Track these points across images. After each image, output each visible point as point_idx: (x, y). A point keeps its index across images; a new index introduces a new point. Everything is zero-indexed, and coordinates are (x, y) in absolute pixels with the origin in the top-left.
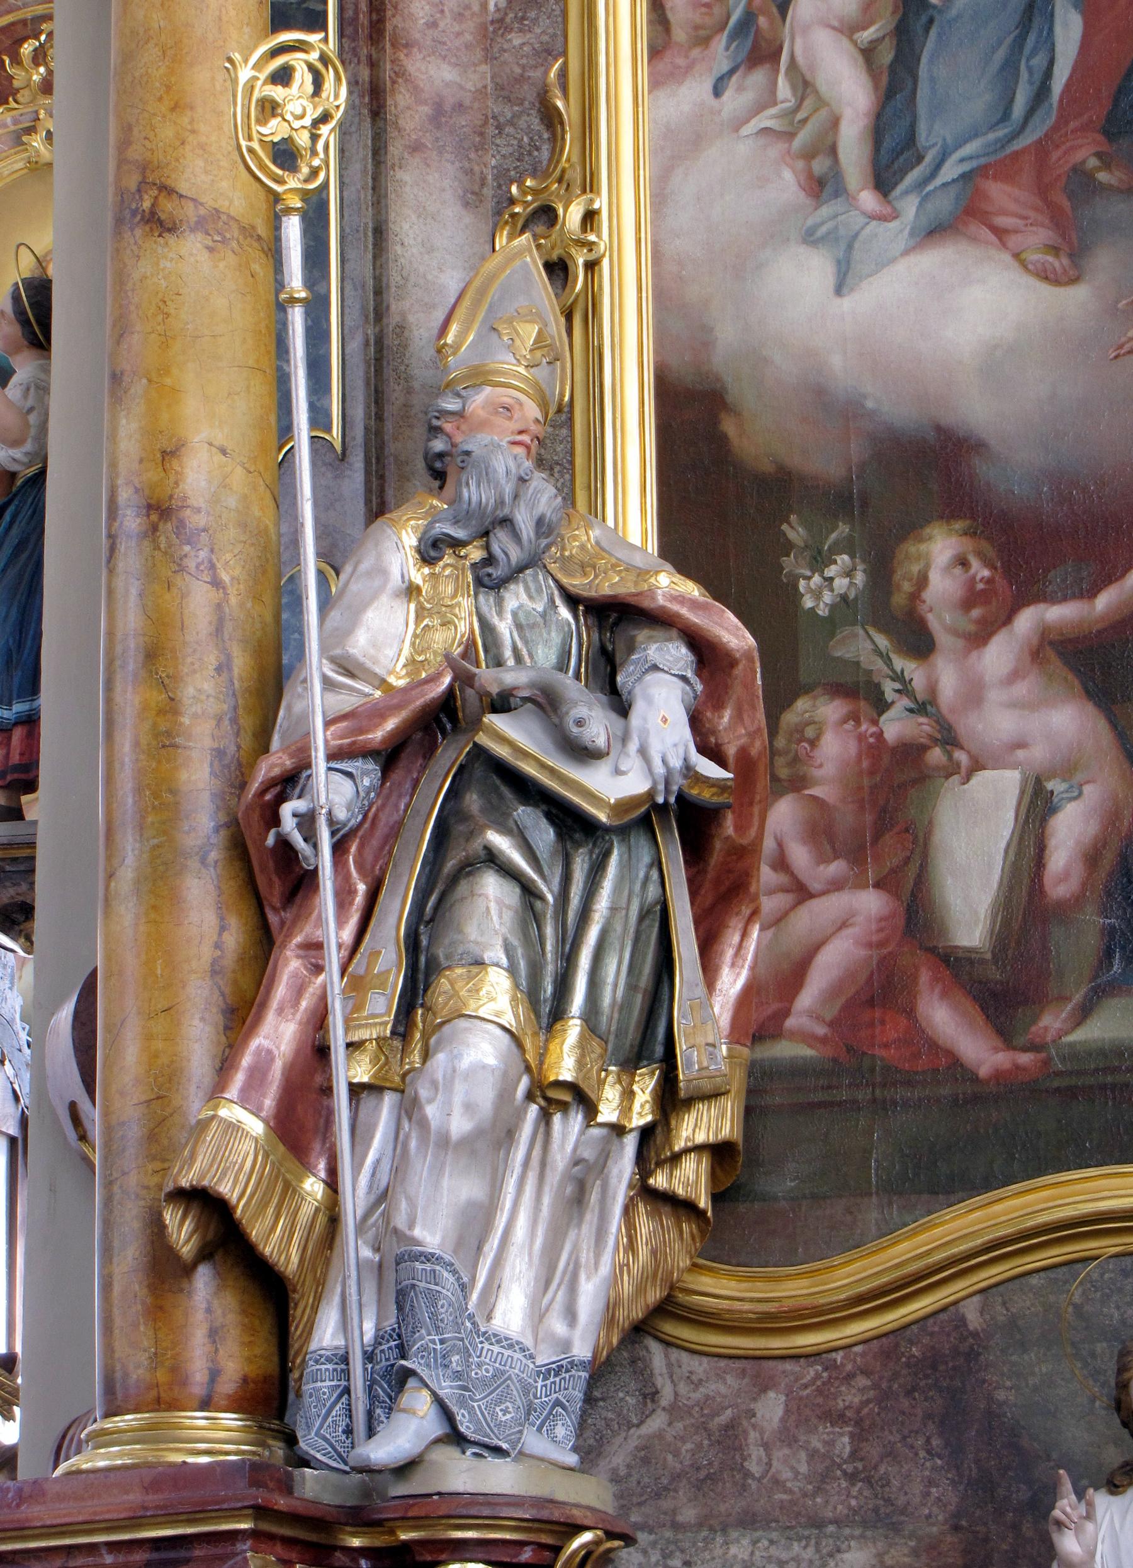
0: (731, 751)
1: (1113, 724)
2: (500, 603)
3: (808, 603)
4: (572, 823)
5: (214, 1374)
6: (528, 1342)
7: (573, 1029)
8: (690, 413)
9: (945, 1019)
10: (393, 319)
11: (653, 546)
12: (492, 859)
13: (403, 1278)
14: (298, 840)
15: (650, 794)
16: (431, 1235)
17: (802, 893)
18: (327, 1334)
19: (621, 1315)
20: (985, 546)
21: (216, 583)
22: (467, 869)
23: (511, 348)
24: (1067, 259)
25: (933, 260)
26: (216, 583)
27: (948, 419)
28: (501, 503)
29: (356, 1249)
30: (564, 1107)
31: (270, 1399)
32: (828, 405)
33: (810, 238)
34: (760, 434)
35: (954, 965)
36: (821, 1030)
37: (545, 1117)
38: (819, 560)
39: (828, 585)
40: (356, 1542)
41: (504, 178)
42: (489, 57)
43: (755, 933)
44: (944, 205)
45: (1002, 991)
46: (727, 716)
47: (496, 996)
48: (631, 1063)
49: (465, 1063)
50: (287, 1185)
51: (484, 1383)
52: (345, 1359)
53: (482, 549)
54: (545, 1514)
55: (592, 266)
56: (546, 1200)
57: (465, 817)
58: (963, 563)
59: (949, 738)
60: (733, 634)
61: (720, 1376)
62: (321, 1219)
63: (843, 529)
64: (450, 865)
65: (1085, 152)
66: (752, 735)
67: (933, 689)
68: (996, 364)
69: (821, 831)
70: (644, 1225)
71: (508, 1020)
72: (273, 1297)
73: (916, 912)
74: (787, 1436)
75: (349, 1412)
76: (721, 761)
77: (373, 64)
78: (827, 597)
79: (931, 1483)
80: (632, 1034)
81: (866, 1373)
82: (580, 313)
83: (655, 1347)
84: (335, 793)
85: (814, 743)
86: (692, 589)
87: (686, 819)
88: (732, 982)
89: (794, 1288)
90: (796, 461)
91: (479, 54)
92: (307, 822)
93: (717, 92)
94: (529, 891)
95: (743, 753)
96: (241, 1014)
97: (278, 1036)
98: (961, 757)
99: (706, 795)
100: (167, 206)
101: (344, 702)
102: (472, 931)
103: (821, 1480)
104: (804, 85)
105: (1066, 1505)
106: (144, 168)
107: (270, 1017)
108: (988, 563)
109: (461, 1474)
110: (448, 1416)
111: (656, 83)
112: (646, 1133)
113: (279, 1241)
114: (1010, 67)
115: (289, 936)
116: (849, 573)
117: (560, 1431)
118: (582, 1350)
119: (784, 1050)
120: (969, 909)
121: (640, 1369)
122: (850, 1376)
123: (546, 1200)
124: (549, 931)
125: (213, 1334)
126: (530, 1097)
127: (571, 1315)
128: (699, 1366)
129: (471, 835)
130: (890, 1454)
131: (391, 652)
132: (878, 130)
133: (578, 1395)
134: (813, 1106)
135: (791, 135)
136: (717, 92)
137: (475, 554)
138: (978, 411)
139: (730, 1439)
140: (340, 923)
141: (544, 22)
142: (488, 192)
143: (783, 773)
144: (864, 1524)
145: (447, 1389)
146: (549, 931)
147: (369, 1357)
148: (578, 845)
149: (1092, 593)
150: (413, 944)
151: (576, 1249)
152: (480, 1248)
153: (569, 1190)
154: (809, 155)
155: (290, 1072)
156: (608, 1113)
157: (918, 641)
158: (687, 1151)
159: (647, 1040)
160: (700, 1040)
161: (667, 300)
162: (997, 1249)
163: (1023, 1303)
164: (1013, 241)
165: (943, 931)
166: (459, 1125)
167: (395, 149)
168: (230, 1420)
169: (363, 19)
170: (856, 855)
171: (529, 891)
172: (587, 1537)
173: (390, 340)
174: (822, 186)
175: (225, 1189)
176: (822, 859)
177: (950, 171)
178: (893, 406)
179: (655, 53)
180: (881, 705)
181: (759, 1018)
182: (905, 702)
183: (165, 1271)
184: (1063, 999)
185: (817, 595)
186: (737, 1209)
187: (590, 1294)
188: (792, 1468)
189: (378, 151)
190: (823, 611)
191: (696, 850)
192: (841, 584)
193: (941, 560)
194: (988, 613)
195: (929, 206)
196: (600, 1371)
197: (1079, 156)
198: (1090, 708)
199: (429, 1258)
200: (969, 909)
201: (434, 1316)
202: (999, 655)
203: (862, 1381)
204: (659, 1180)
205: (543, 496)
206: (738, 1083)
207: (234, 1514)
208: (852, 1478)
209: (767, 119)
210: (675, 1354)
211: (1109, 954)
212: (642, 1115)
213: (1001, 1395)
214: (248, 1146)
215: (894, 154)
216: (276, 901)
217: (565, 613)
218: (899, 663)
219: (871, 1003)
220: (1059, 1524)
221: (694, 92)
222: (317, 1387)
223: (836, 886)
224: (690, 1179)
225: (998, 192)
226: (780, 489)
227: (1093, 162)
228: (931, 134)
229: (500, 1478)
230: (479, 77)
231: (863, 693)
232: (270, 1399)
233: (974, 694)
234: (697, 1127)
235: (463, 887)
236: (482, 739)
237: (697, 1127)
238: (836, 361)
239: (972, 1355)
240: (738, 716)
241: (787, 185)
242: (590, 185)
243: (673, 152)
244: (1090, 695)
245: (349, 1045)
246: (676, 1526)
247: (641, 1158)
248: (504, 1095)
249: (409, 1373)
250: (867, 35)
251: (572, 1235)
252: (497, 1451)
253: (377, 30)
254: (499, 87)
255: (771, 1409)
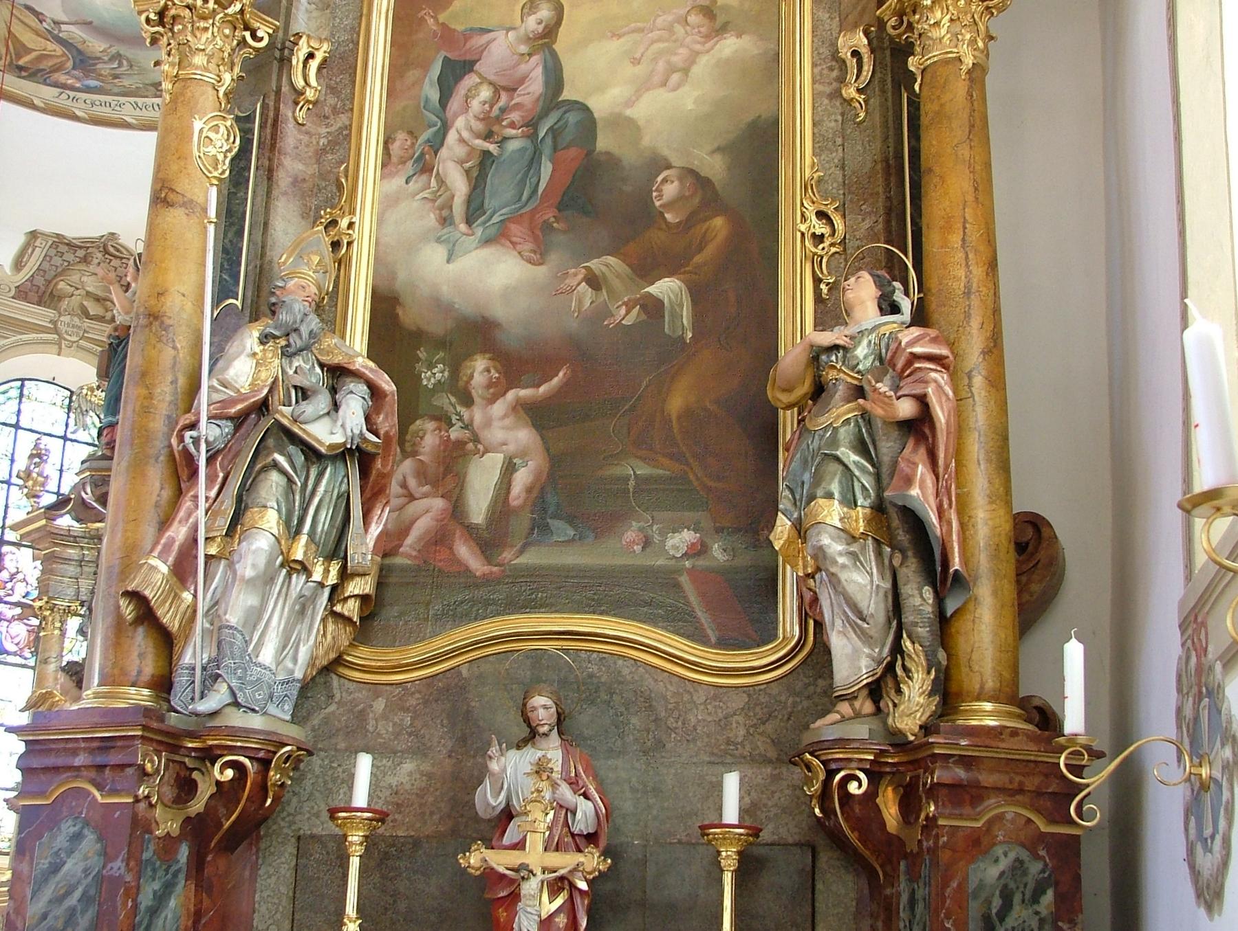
0: (382, 432)
1: (543, 439)
2: (291, 363)
3: (425, 382)
4: (312, 453)
5: (140, 672)
6: (273, 667)
7: (304, 539)
8: (385, 305)
9: (465, 552)
10: (267, 259)
11: (365, 353)
12: (275, 465)
13: (219, 633)
14: (192, 449)
15: (344, 444)
16: (233, 618)
17: (411, 498)
18: (187, 659)
19: (317, 662)
20: (497, 364)
21: (175, 348)
22: (265, 469)
23: (307, 264)
24: (539, 255)
25: (486, 252)
26: (175, 348)
27: (487, 314)
28: (295, 322)
29: (200, 623)
30: (298, 571)
31: (163, 685)
32: (441, 306)
33: (438, 240)
34: (410, 316)
35: (471, 531)
36: (414, 553)
37: (289, 575)
38: (431, 366)
39: (434, 375)
40: (190, 745)
41: (318, 209)
42: (318, 162)
43: (387, 510)
44: (492, 231)
45: (488, 543)
46: (381, 417)
47: (270, 521)
48: (329, 558)
49: (253, 547)
50: (176, 595)
51: (252, 682)
52: (194, 669)
53: (286, 343)
54: (269, 738)
55: (349, 244)
56: (286, 610)
57: (266, 448)
58: (489, 371)
59: (476, 440)
60: (386, 384)
61: (360, 691)
62: (189, 610)
63: (442, 354)
64: (258, 466)
65: (549, 215)
66: (392, 427)
67: (472, 420)
68: (508, 294)
69: (422, 474)
70: (331, 627)
71: (275, 532)
72: (167, 642)
73: (457, 510)
74: (385, 716)
75: (194, 691)
76: (378, 437)
77: (270, 160)
78: (433, 380)
79: (442, 738)
80: (331, 545)
81: (420, 692)
82: (342, 264)
83: (334, 677)
84: (210, 431)
85: (422, 438)
86: (371, 364)
87: (358, 456)
88: (375, 530)
89: (394, 656)
90: (425, 327)
91: (314, 161)
92: (196, 441)
93: (407, 182)
94: (290, 481)
95: (387, 433)
96: (165, 523)
97: (178, 532)
98: (480, 447)
99: (370, 449)
100: (171, 196)
101: (217, 397)
102: (263, 493)
103: (397, 735)
104: (441, 182)
105: (494, 750)
106: (163, 181)
107: (176, 524)
108: (497, 371)
109: (237, 719)
110: (233, 694)
111: (382, 178)
112: (334, 588)
113: (169, 617)
114: (522, 183)
115: (188, 491)
116: (442, 372)
117: (286, 707)
118: (299, 675)
119: (398, 560)
120: (479, 506)
121: (327, 685)
122: (413, 693)
123: (286, 610)
124: (297, 498)
125: (141, 655)
126: (282, 565)
127: (295, 660)
128: (352, 686)
129: (268, 455)
130: (425, 725)
131: (244, 379)
132: (469, 201)
133: (295, 693)
134: (408, 584)
135: (434, 201)
136: (407, 182)
137: (283, 343)
138: (499, 312)
139: (362, 716)
140: (208, 488)
141: (342, 151)
142: (312, 213)
143: (409, 449)
144: (414, 753)
145: (234, 684)
146: (297, 498)
147: (204, 669)
148: (313, 463)
149: (539, 386)
150: (239, 499)
151: (300, 633)
152: (255, 626)
153: (297, 607)
154: (441, 208)
155: (181, 546)
156: (317, 576)
157: (468, 401)
158: (350, 597)
159: (336, 550)
160: (359, 551)
161: (380, 262)
162: (476, 645)
163: (486, 667)
164: (518, 247)
165: (467, 517)
166: (249, 573)
167: (275, 193)
168: (146, 692)
169: (268, 142)
170: (435, 483)
171: (290, 481)
172: (288, 748)
173: (266, 267)
174: (446, 221)
175: (147, 593)
176: (421, 485)
177: (496, 219)
178: (465, 306)
179: (384, 166)
180: (451, 425)
181: (388, 546)
182: (460, 424)
183: (119, 627)
184: (512, 546)
185: (429, 380)
186: (369, 622)
187: (304, 652)
188: (386, 729)
189: (269, 193)
190: (430, 386)
191: (364, 473)
192: (439, 376)
193: (479, 370)
194: (496, 391)
195: (487, 231)
196: (306, 687)
197: (546, 217)
198: (534, 431)
199: (231, 627)
200: (479, 506)
201: (232, 652)
202: (499, 408)
203: (417, 695)
204: (338, 608)
205: (314, 323)
206: (374, 571)
207: (132, 728)
208: (410, 734)
209: (425, 194)
210: (342, 680)
211: (533, 529)
212: (332, 579)
213: (473, 704)
214: (160, 576)
215: (474, 211)
216: (185, 478)
217: (318, 370)
218: (459, 408)
219: (436, 543)
220: (490, 757)
221: (398, 182)
222: (181, 679)
223: (425, 496)
224: (351, 608)
225: (514, 228)
226: (418, 337)
227: (552, 219)
228: (490, 204)
229: (256, 722)
230: (313, 169)
231: (443, 419)
232: (163, 685)
233: (488, 423)
234: (357, 587)
235: (262, 476)
236: (277, 416)
237: (357, 587)
238: (445, 288)
239: (463, 688)
240: (386, 418)
241: (432, 219)
242: (352, 212)
243: (387, 204)
244: (534, 426)
245: (206, 539)
246: (336, 750)
247: (330, 599)
248: (270, 562)
249: (219, 676)
250: (468, 165)
251: (299, 627)
252: (253, 710)
253: (273, 146)
254: (321, 174)
255: (380, 705)
